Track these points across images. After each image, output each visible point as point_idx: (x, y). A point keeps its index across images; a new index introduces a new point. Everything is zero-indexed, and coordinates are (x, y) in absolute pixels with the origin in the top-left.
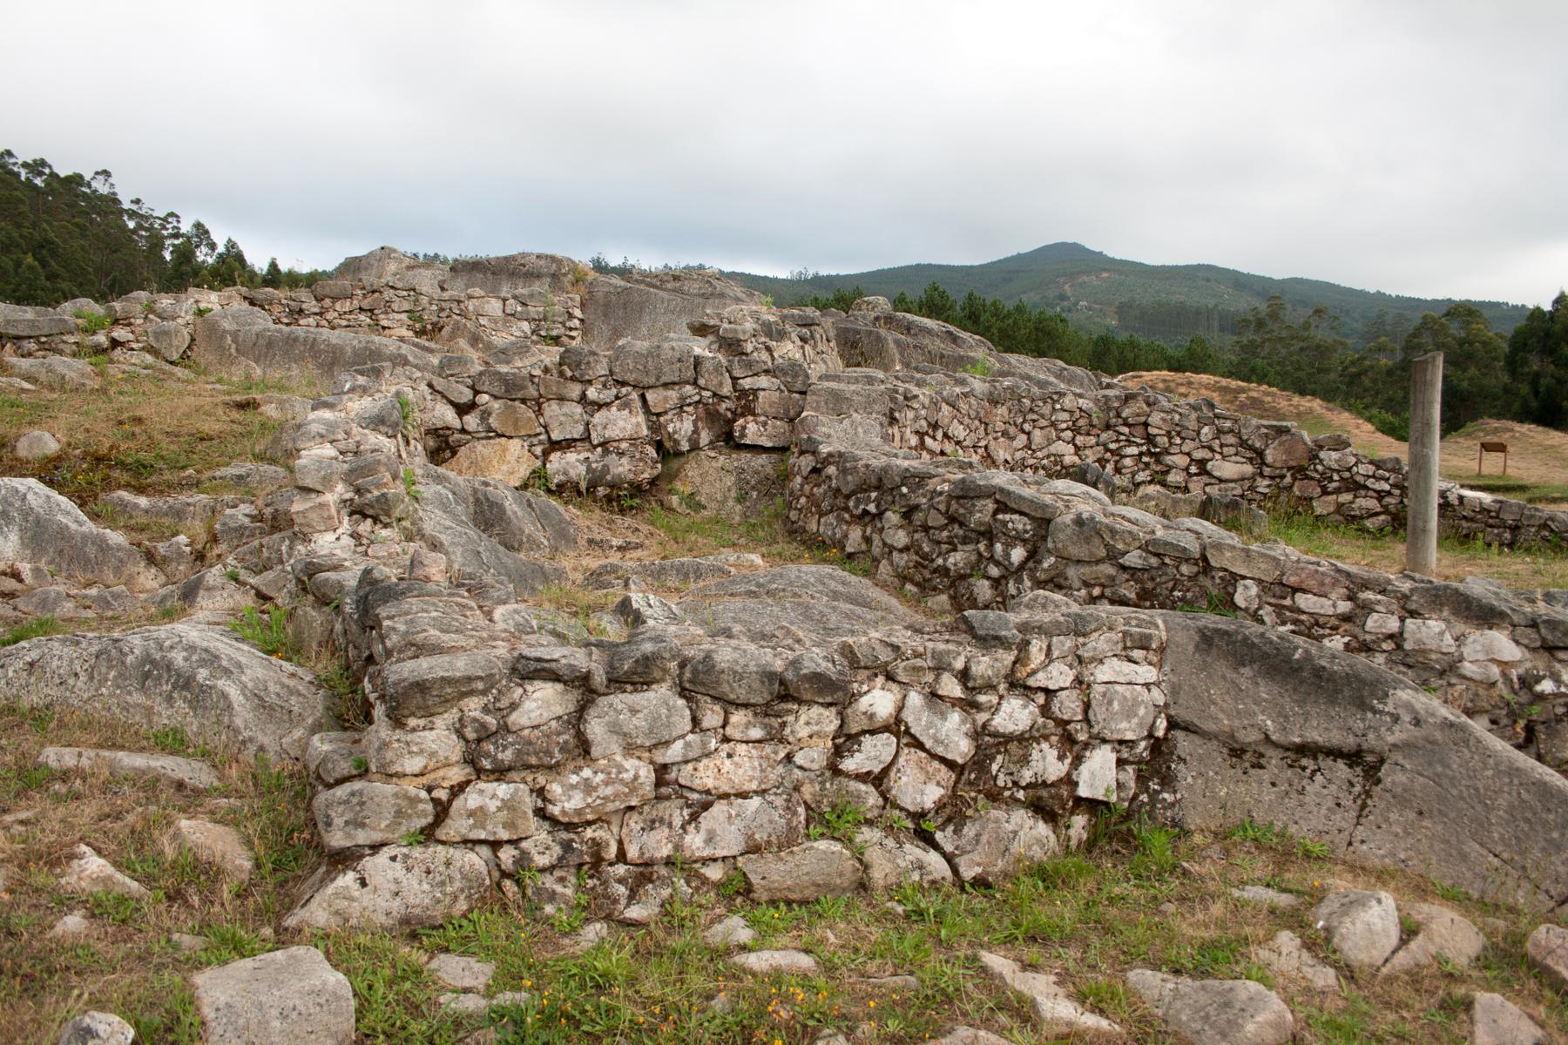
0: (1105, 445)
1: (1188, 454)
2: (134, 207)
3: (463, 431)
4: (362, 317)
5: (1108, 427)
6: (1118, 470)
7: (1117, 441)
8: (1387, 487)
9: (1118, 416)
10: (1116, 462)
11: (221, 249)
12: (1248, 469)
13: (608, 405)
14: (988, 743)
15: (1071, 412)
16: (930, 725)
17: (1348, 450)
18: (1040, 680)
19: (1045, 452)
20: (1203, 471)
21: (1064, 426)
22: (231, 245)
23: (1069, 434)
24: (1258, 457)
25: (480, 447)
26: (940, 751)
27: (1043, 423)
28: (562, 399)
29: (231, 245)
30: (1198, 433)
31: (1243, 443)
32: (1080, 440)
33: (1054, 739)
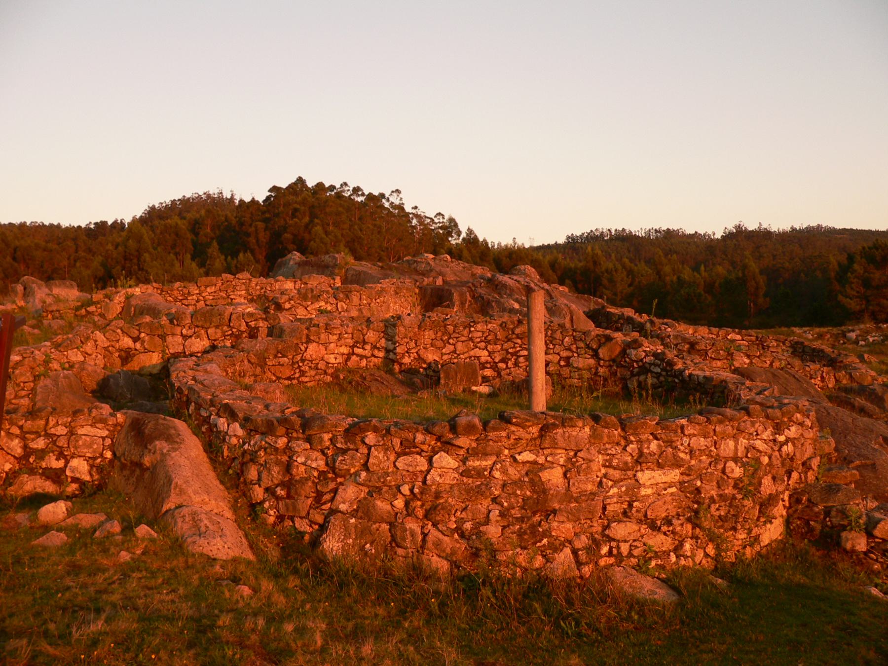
0: (507, 350)
1: (558, 354)
2: (414, 211)
3: (136, 350)
4: (222, 294)
5: (509, 340)
6: (516, 364)
7: (514, 347)
8: (659, 370)
9: (513, 333)
10: (516, 360)
11: (463, 235)
12: (592, 362)
13: (191, 337)
14: (28, 452)
15: (483, 333)
16: (7, 442)
17: (640, 349)
18: (53, 431)
19: (466, 355)
20: (568, 364)
21: (479, 340)
22: (470, 232)
23: (483, 345)
24: (595, 355)
25: (141, 356)
26: (9, 451)
27: (464, 339)
28: (173, 334)
29: (470, 232)
30: (563, 341)
31: (588, 346)
32: (490, 348)
33: (56, 453)
